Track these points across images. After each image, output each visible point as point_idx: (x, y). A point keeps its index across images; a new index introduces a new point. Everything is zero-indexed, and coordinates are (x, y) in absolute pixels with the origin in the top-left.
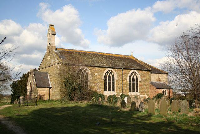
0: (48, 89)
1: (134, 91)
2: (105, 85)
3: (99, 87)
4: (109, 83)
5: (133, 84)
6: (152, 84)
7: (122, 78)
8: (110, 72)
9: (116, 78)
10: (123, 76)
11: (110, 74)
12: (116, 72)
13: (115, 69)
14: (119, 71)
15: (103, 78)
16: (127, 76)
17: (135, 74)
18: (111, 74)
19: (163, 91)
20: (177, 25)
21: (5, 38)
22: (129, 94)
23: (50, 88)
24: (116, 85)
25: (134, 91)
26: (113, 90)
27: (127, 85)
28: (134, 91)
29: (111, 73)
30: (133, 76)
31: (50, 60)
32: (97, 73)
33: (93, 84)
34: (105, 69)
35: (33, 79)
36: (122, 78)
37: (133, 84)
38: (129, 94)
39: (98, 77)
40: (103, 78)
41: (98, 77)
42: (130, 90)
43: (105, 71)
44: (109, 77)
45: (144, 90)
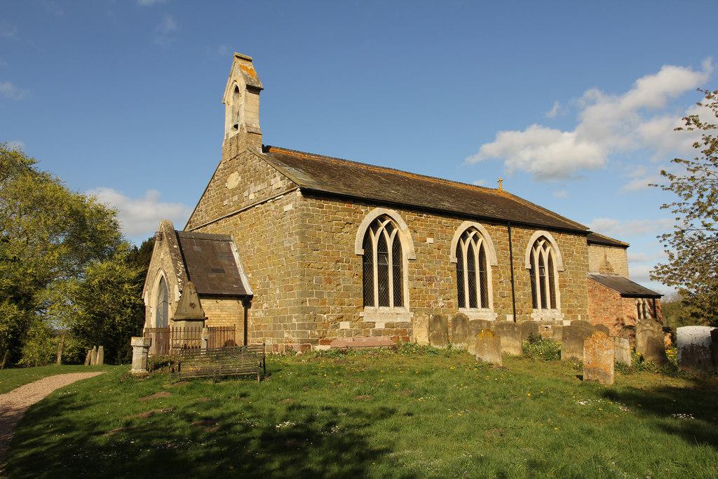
0: (234, 306)
1: (387, 304)
3: (443, 292)
5: (542, 279)
6: (595, 278)
8: (386, 222)
9: (407, 248)
11: (385, 232)
12: (490, 234)
15: (451, 256)
17: (476, 238)
22: (532, 316)
24: (494, 284)
28: (387, 304)
29: (389, 228)
30: (382, 237)
31: (241, 189)
32: (431, 235)
33: (422, 279)
35: (175, 262)
37: (542, 279)
38: (532, 316)
40: (453, 258)
41: (436, 252)
42: (368, 301)
43: (456, 229)
44: (382, 240)
45: (574, 302)
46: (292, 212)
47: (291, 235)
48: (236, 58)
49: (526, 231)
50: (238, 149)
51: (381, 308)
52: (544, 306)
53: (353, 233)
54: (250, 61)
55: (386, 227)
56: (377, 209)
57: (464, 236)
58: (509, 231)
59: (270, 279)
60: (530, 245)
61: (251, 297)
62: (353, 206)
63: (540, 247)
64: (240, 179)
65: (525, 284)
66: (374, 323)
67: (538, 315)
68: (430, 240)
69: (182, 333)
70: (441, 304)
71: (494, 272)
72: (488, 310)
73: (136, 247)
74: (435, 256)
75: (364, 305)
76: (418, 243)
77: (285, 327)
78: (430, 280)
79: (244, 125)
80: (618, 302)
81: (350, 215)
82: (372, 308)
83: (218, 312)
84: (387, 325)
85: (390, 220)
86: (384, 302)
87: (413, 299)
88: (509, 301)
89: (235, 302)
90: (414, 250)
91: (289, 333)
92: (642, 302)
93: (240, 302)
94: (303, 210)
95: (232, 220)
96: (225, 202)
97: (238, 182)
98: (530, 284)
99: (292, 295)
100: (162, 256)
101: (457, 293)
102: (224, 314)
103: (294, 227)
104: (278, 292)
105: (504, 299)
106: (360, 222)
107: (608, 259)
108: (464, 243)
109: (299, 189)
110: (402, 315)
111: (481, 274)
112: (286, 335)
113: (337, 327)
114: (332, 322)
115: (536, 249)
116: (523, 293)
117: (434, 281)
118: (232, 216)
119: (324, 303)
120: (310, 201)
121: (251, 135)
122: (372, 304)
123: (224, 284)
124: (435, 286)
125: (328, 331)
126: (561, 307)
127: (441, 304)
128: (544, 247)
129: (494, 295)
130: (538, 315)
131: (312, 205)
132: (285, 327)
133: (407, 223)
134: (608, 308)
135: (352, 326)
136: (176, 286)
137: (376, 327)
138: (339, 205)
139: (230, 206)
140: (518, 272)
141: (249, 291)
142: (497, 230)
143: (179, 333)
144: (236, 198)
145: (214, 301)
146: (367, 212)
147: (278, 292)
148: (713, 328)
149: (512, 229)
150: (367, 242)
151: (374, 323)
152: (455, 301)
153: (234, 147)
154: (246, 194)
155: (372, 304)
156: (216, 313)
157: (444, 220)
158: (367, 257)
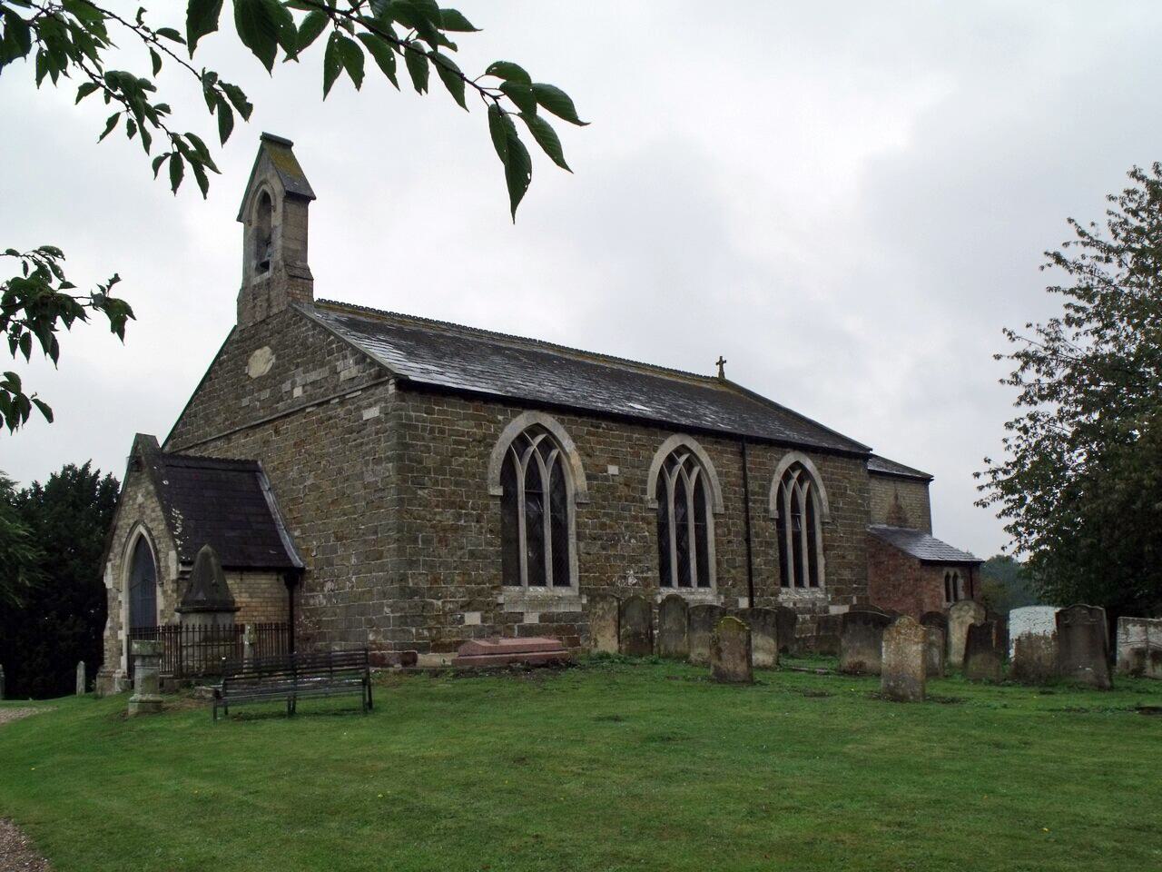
4: (682, 530)
5: (797, 537)
7: (746, 501)
8: (540, 438)
9: (577, 482)
11: (539, 457)
16: (765, 490)
17: (689, 465)
18: (689, 472)
19: (947, 577)
20: (1028, 326)
21: (1050, 289)
22: (781, 598)
28: (542, 583)
30: (533, 463)
32: (614, 461)
36: (746, 501)
37: (797, 537)
39: (622, 491)
43: (655, 450)
46: (377, 420)
47: (378, 461)
50: (269, 306)
51: (531, 589)
52: (799, 583)
53: (485, 456)
57: (671, 461)
59: (338, 539)
60: (777, 478)
61: (302, 571)
63: (792, 483)
64: (274, 360)
65: (769, 544)
67: (790, 596)
69: (197, 634)
70: (631, 580)
72: (708, 590)
73: (36, 485)
76: (834, 495)
77: (370, 623)
79: (281, 263)
80: (917, 574)
84: (542, 618)
86: (538, 579)
87: (584, 568)
88: (741, 575)
91: (377, 633)
92: (952, 574)
93: (281, 577)
94: (400, 417)
95: (259, 435)
96: (245, 402)
97: (270, 365)
98: (776, 545)
99: (382, 568)
100: (140, 499)
101: (657, 561)
103: (386, 447)
104: (353, 561)
107: (903, 503)
108: (689, 476)
109: (392, 381)
110: (566, 599)
111: (697, 527)
112: (371, 637)
115: (801, 485)
116: (764, 562)
118: (259, 425)
124: (621, 549)
126: (826, 583)
127: (631, 580)
128: (801, 481)
129: (718, 563)
130: (790, 596)
132: (370, 623)
134: (900, 585)
135: (484, 620)
136: (173, 554)
139: (254, 409)
140: (758, 524)
141: (297, 561)
143: (191, 634)
144: (266, 394)
146: (507, 422)
147: (353, 561)
148: (1058, 609)
152: (654, 574)
153: (261, 301)
154: (286, 387)
156: (242, 600)
158: (509, 499)
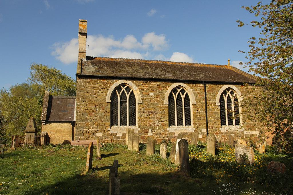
0: (69, 126)
1: (232, 124)
2: (113, 112)
8: (230, 91)
9: (192, 101)
10: (208, 96)
11: (180, 93)
12: (192, 89)
13: (191, 85)
14: (199, 87)
15: (165, 101)
23: (73, 124)
24: (194, 113)
25: (230, 123)
26: (188, 123)
27: (217, 113)
28: (232, 124)
29: (232, 93)
33: (145, 112)
34: (168, 84)
39: (155, 99)
40: (166, 101)
43: (169, 87)
44: (229, 99)
48: (80, 22)
49: (217, 86)
53: (105, 93)
54: (86, 22)
55: (230, 93)
56: (120, 81)
58: (205, 87)
62: (106, 81)
66: (116, 133)
68: (151, 94)
70: (157, 124)
71: (194, 108)
74: (154, 101)
75: (221, 125)
78: (151, 113)
81: (104, 85)
82: (116, 126)
83: (60, 128)
85: (128, 85)
87: (140, 122)
89: (68, 124)
90: (141, 99)
93: (71, 124)
102: (63, 129)
105: (200, 121)
106: (110, 87)
113: (95, 135)
114: (92, 133)
116: (215, 117)
117: (153, 113)
119: (88, 124)
120: (82, 80)
121: (80, 54)
122: (225, 124)
123: (65, 117)
125: (90, 137)
127: (157, 124)
129: (194, 119)
131: (83, 82)
133: (138, 86)
137: (117, 135)
138: (98, 81)
140: (210, 107)
142: (198, 86)
145: (58, 124)
149: (207, 85)
150: (171, 97)
151: (116, 133)
155: (225, 124)
157: (161, 84)
158: (222, 106)
